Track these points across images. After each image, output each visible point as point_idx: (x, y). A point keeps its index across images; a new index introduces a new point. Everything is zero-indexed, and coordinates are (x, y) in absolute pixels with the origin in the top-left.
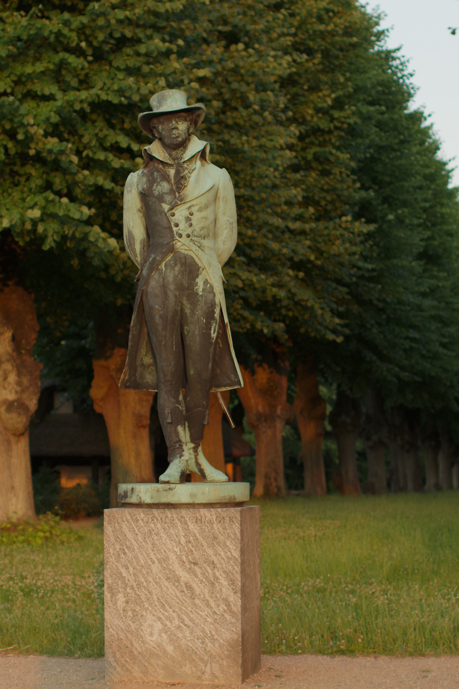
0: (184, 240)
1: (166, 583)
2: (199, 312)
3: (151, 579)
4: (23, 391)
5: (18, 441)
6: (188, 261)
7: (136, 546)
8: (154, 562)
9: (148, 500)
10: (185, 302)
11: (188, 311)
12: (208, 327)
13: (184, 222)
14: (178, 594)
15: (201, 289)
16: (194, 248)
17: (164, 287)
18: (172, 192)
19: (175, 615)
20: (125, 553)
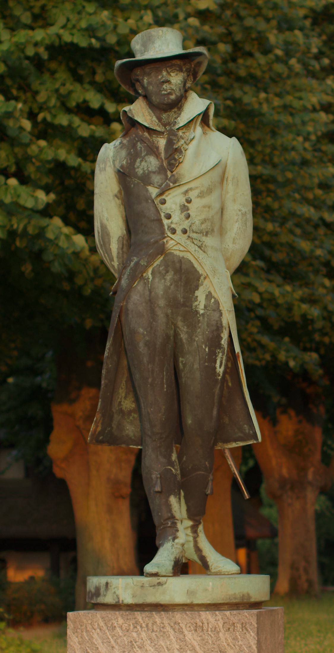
0: (179, 237)
9: (128, 600)
10: (180, 324)
11: (184, 336)
12: (212, 358)
15: (202, 306)
16: (193, 248)
17: (151, 302)
18: (161, 170)
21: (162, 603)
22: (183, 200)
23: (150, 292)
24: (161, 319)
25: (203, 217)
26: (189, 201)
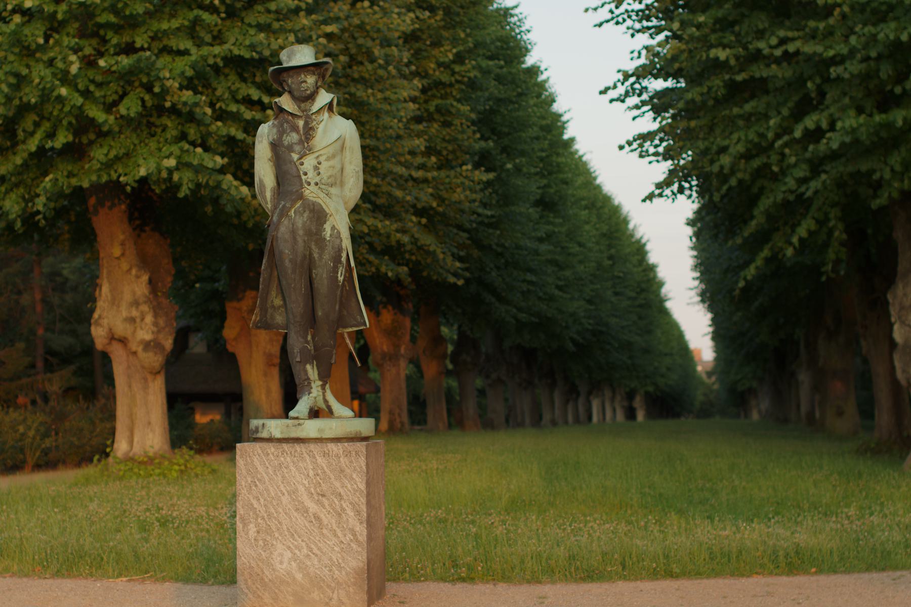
0: (312, 187)
1: (296, 514)
2: (326, 257)
3: (281, 510)
4: (159, 332)
10: (313, 247)
11: (316, 255)
12: (335, 270)
15: (328, 235)
16: (322, 195)
17: (293, 232)
18: (301, 142)
19: (304, 544)
20: (256, 486)
26: (319, 163)
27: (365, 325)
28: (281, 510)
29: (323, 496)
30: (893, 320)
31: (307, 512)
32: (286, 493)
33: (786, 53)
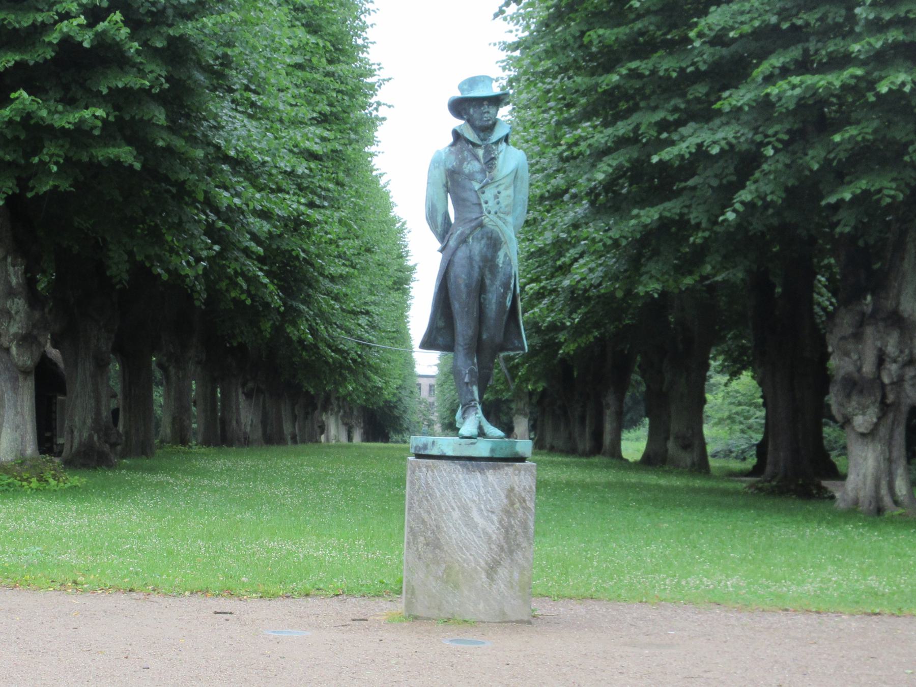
0: (492, 216)
1: (465, 529)
2: (498, 283)
3: (451, 525)
4: (34, 326)
5: (25, 379)
6: (494, 235)
7: (438, 494)
8: (454, 509)
9: (450, 453)
10: (487, 273)
11: (488, 282)
12: (504, 296)
13: (492, 199)
14: (476, 539)
15: (501, 262)
16: (500, 223)
17: (470, 258)
18: (483, 171)
19: (471, 558)
20: (427, 501)
21: (123, 599)
22: (496, 192)
23: (470, 251)
24: (477, 269)
25: (506, 203)
26: (499, 193)
27: (523, 349)
28: (451, 525)
29: (493, 512)
30: (830, 349)
31: (476, 527)
32: (457, 509)
33: (793, 26)
